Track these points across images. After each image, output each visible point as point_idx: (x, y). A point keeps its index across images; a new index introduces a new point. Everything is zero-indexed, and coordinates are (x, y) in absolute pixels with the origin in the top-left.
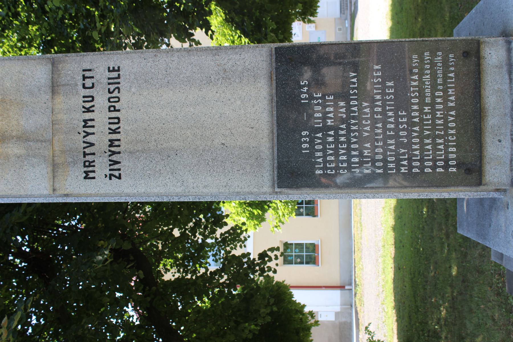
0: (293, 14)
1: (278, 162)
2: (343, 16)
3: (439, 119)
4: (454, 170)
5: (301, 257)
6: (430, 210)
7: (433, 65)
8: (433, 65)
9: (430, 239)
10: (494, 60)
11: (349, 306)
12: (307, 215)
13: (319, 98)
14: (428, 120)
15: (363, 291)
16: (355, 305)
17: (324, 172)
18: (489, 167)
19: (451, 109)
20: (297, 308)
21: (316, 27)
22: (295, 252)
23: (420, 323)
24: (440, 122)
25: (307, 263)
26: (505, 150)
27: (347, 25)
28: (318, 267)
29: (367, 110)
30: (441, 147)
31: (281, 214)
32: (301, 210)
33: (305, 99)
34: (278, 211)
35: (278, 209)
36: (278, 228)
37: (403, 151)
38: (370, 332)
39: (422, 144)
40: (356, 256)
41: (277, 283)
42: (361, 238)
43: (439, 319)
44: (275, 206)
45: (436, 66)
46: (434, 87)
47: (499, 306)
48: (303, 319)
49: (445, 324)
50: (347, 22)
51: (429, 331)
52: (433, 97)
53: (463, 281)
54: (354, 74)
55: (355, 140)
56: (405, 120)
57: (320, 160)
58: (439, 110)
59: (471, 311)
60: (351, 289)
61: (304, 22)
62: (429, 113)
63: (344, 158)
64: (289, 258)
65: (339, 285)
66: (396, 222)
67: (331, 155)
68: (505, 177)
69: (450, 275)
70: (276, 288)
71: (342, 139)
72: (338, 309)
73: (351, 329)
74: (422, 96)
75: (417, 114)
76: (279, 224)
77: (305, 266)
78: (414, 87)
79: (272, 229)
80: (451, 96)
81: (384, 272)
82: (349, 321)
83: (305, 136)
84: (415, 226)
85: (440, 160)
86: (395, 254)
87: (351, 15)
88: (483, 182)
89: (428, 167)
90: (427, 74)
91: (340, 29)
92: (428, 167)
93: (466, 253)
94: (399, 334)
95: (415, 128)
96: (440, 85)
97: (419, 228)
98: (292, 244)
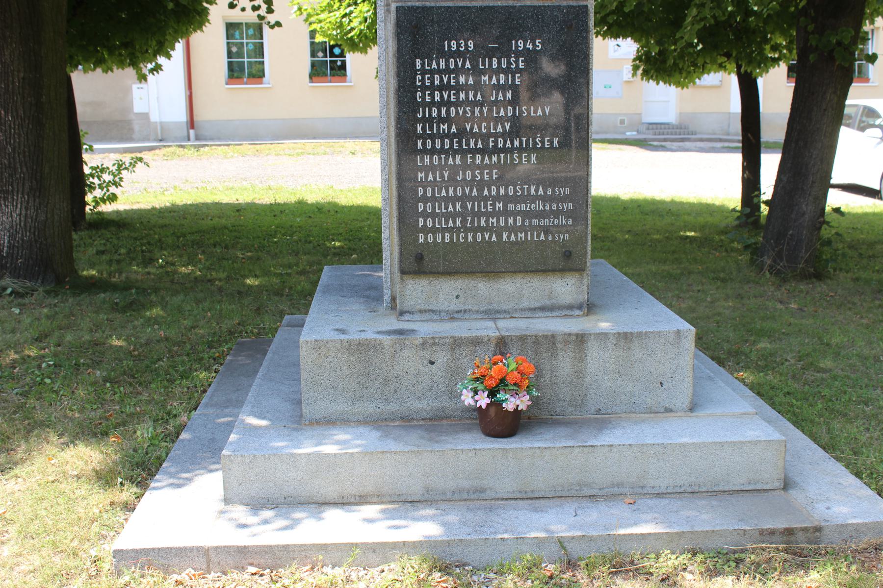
0: (648, 42)
1: (432, 7)
2: (645, 127)
3: (487, 221)
4: (421, 240)
5: (240, 54)
6: (338, 250)
7: (556, 214)
8: (556, 214)
9: (294, 251)
10: (559, 289)
11: (162, 137)
12: (313, 65)
13: (517, 65)
14: (486, 207)
15: (188, 158)
16: (165, 146)
17: (419, 70)
18: (424, 283)
19: (499, 236)
20: (167, 44)
21: (628, 82)
22: (247, 44)
23: (160, 240)
24: (483, 222)
25: (230, 64)
26: (446, 304)
27: (628, 133)
28: (224, 82)
29: (500, 129)
30: (451, 224)
31: (322, 16)
32: (320, 54)
33: (517, 46)
34: (326, 13)
35: (330, 12)
36: (298, 13)
37: (446, 175)
38: (134, 166)
39: (454, 200)
40: (246, 147)
41: (205, 12)
42: (277, 155)
43: (173, 264)
44: (336, 7)
45: (555, 217)
46: (527, 215)
47: (214, 333)
48: (147, 55)
49: (167, 272)
50: (635, 133)
51: (150, 252)
52: (515, 214)
53: (239, 293)
54: (547, 112)
55: (461, 113)
56: (486, 177)
57: (434, 66)
58: (498, 221)
59: (198, 302)
60: (189, 140)
61: (634, 60)
62: (494, 209)
63: (437, 98)
64: (237, 33)
65: (195, 119)
66: (312, 205)
67: (442, 80)
68: (412, 303)
69: (245, 277)
70: (199, 8)
71: (462, 96)
72: (154, 118)
73: (122, 140)
74: (516, 199)
75: (494, 193)
76: (305, 13)
77: (225, 60)
78: (529, 189)
79: (295, 2)
80: (516, 235)
81: (227, 189)
82: (134, 136)
83: (466, 45)
84: (310, 231)
85: (434, 222)
86: (262, 205)
87: (645, 140)
88: (405, 277)
89: (425, 207)
90: (544, 206)
91: (622, 122)
92: (425, 207)
93: (282, 295)
94: (133, 211)
95: (475, 190)
96: (530, 223)
97: (308, 236)
98: (262, 38)
